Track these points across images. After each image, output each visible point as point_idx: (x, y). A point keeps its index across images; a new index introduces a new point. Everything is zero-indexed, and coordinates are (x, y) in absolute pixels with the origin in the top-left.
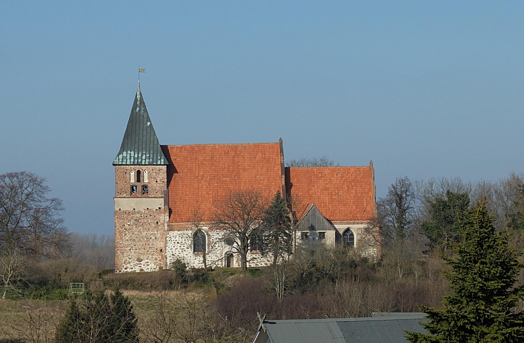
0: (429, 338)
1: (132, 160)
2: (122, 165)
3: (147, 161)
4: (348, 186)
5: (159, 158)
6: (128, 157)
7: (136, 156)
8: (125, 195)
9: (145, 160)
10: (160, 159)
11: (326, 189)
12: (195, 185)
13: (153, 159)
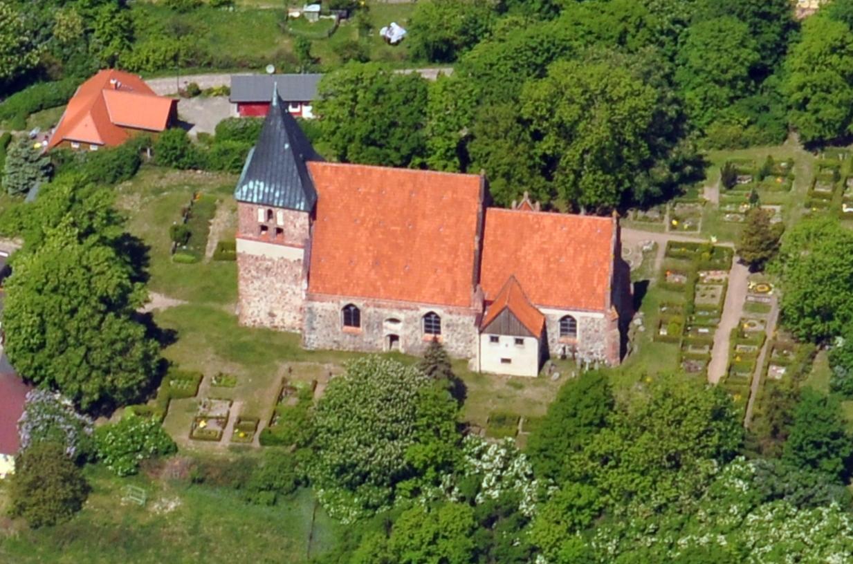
0: (800, 326)
1: (261, 197)
2: (245, 202)
3: (282, 201)
4: (575, 250)
5: (298, 199)
6: (256, 191)
7: (267, 190)
8: (251, 235)
9: (279, 198)
10: (300, 202)
11: (543, 251)
12: (351, 234)
13: (290, 199)
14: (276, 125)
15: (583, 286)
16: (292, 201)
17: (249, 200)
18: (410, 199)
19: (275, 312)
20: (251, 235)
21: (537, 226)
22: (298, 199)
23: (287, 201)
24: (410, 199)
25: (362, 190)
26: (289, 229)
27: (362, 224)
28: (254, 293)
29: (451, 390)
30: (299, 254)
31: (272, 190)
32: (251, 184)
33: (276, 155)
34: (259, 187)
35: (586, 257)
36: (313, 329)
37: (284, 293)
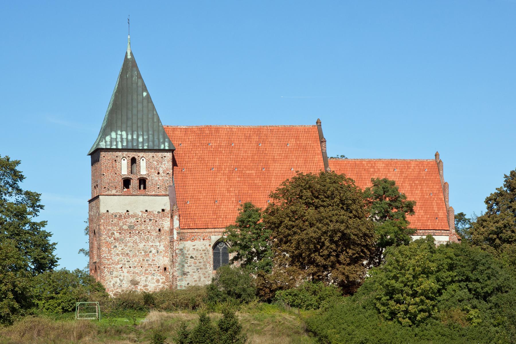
1: (125, 144)
5: (162, 140)
6: (119, 139)
7: (130, 137)
8: (114, 192)
9: (143, 143)
13: (153, 142)
14: (132, 76)
15: (426, 212)
16: (156, 142)
17: (114, 147)
18: (258, 148)
19: (138, 279)
20: (114, 192)
21: (372, 170)
22: (162, 140)
23: (151, 143)
24: (258, 148)
25: (213, 144)
26: (153, 179)
27: (218, 171)
28: (116, 259)
29: (342, 274)
30: (165, 203)
31: (135, 137)
32: (113, 135)
33: (135, 104)
34: (121, 135)
35: (422, 190)
36: (184, 274)
37: (147, 253)
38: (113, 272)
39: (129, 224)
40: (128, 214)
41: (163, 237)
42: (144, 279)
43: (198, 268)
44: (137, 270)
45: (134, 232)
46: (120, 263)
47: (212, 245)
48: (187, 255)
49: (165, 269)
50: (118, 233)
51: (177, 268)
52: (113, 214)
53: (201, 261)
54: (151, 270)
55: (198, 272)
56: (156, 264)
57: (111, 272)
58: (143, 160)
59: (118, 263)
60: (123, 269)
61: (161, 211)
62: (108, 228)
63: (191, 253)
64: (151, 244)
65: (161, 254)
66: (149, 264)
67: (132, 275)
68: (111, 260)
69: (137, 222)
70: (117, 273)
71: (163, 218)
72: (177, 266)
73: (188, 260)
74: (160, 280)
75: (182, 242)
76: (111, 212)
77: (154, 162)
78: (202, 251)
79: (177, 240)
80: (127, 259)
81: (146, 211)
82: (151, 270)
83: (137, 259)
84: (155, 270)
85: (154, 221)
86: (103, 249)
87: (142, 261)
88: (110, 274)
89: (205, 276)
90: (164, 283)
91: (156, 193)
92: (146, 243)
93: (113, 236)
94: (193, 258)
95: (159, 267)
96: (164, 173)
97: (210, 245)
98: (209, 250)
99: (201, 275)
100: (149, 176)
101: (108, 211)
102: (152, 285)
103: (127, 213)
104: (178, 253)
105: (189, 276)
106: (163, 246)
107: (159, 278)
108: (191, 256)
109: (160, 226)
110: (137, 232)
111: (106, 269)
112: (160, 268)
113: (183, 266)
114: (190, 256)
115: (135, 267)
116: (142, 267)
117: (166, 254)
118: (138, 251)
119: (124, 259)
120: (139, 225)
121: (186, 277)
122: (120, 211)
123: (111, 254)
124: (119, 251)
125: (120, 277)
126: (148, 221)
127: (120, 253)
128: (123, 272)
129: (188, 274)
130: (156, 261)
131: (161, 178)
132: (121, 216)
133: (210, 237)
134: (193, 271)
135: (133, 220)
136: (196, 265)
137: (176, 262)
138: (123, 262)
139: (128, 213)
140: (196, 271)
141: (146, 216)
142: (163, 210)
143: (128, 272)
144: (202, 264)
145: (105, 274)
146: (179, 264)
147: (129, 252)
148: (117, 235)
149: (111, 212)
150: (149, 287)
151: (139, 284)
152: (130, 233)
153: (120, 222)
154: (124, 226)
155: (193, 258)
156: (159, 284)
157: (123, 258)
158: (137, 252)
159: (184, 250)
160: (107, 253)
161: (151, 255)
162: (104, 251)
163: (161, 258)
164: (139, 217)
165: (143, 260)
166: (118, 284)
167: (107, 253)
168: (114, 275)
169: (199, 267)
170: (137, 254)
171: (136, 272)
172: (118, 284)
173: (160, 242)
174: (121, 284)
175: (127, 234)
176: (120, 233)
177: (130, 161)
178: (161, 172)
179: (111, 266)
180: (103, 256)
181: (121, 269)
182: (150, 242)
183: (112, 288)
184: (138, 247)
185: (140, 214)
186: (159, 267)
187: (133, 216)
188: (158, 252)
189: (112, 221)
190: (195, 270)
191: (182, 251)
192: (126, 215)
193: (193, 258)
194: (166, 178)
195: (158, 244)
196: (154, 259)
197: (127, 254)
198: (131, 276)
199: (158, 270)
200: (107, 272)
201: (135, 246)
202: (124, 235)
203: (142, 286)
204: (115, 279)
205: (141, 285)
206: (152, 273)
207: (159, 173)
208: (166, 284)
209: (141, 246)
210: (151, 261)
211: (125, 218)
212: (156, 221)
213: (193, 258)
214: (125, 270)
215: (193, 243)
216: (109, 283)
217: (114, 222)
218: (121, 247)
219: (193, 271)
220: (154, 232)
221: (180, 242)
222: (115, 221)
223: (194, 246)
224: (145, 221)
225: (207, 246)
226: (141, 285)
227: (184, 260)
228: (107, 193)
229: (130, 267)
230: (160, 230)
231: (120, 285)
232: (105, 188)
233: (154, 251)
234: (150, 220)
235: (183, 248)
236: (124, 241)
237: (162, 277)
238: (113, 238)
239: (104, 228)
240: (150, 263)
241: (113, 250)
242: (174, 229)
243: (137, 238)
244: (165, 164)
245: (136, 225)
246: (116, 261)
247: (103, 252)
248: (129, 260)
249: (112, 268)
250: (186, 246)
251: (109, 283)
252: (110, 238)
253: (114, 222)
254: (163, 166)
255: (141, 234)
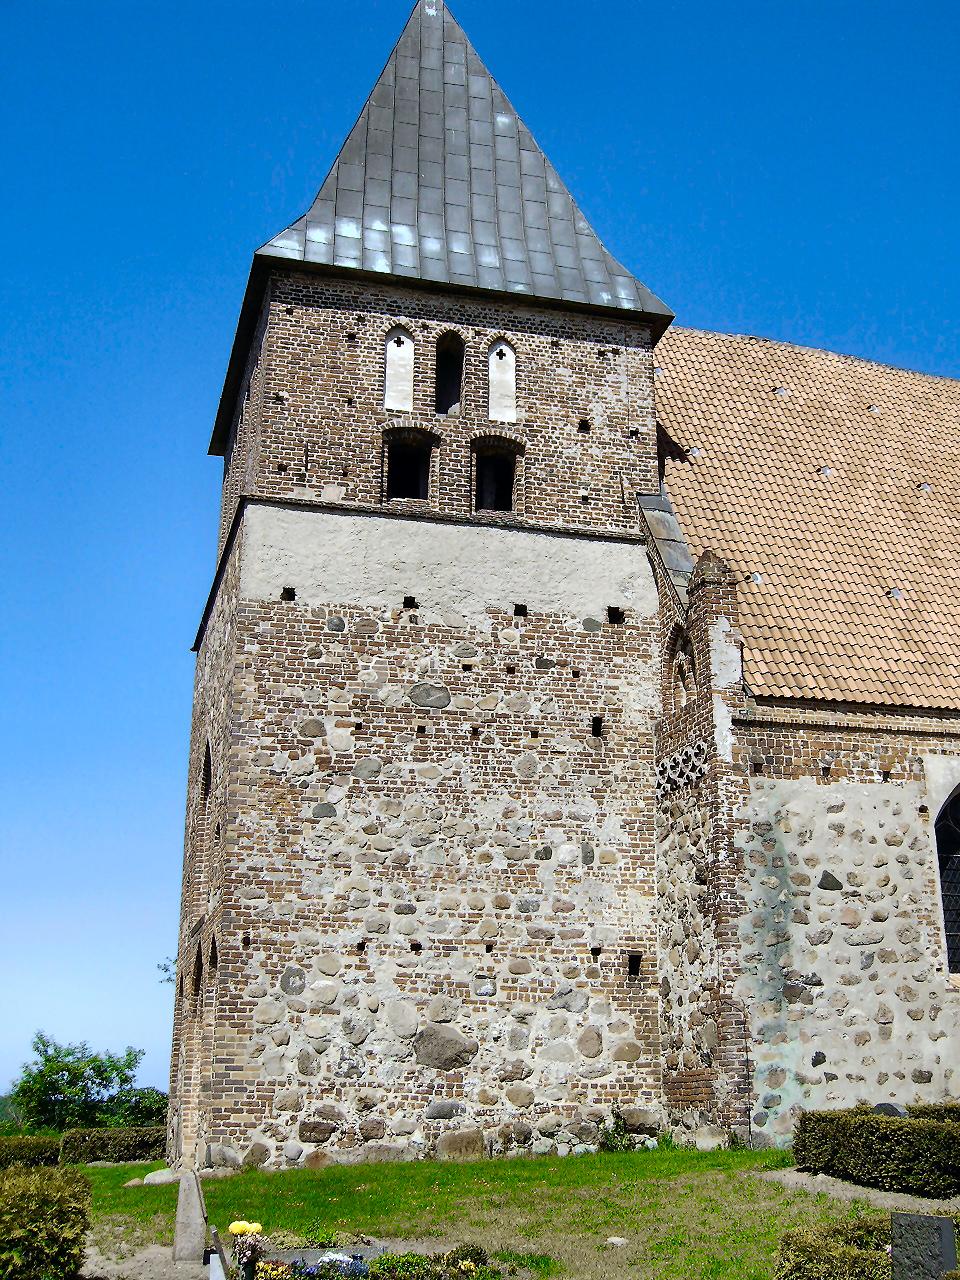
8: (333, 494)
19: (462, 1025)
28: (330, 890)
36: (792, 990)
38: (301, 976)
39: (416, 678)
40: (413, 619)
41: (617, 769)
42: (508, 1028)
43: (869, 949)
44: (459, 968)
45: (444, 725)
46: (350, 914)
47: (934, 813)
48: (803, 869)
49: (634, 963)
50: (349, 725)
51: (747, 949)
52: (318, 613)
53: (884, 905)
54: (546, 971)
55: (873, 977)
56: (581, 934)
57: (292, 972)
58: (501, 355)
59: (336, 920)
60: (372, 956)
61: (602, 617)
62: (288, 692)
63: (822, 857)
64: (550, 807)
65: (608, 870)
66: (535, 933)
67: (426, 996)
68: (292, 896)
69: (467, 668)
70: (328, 982)
71: (618, 660)
72: (747, 939)
73: (811, 901)
74: (606, 1033)
75: (759, 778)
76: (309, 599)
77: (559, 371)
78: (881, 841)
79: (736, 768)
80: (397, 894)
81: (521, 610)
82: (546, 971)
83: (464, 899)
84: (571, 973)
85: (567, 672)
86: (246, 819)
87: (490, 909)
88: (285, 987)
89: (912, 1006)
90: (627, 1054)
91: (572, 526)
92: (516, 796)
93: (318, 742)
94: (837, 886)
95: (596, 952)
96: (612, 428)
97: (923, 809)
98: (922, 838)
99: (891, 1000)
100: (533, 434)
101: (289, 594)
102: (555, 1066)
103: (405, 616)
104: (748, 847)
105: (820, 1006)
106: (618, 820)
107: (595, 1019)
108: (827, 876)
109: (600, 704)
110: (467, 726)
111: (262, 955)
112: (601, 957)
113: (783, 938)
114: (815, 874)
115: (449, 948)
116: (489, 949)
117: (640, 873)
118: (470, 847)
119: (378, 892)
120: (477, 691)
121: (802, 1015)
122: (368, 601)
123: (295, 855)
124: (351, 842)
125: (347, 1012)
126: (528, 666)
127: (353, 851)
128: (370, 980)
129: (816, 990)
130: (576, 912)
131: (595, 451)
132: (368, 625)
133: (920, 761)
134: (842, 969)
135: (438, 658)
136: (857, 935)
137: (738, 912)
138: (370, 913)
139: (411, 612)
140: (858, 972)
141: (517, 642)
142: (615, 615)
143: (400, 980)
144: (892, 925)
145: (252, 987)
146: (759, 924)
147: (413, 851)
148: (339, 738)
149: (309, 599)
150: (533, 1080)
151: (475, 1060)
152: (421, 729)
153: (360, 663)
154: (389, 687)
155: (838, 886)
156: (601, 1062)
157: (373, 884)
158: (460, 851)
159: (778, 832)
160: (271, 847)
161: (545, 871)
162: (249, 836)
163: (608, 891)
164: (479, 639)
165: (502, 905)
166: (333, 1055)
167: (271, 847)
168: (307, 998)
169: (874, 948)
170: (464, 861)
171: (456, 978)
172: (333, 1055)
173: (598, 795)
174: (356, 1060)
175: (403, 739)
176: (358, 726)
177: (431, 350)
178: (597, 422)
179: (292, 936)
180: (243, 868)
181: (355, 960)
182: (542, 795)
183: (295, 1087)
184: (469, 820)
185: (486, 625)
186: (596, 952)
187: (443, 635)
188: (588, 858)
189: (315, 654)
190: (855, 968)
191: (769, 835)
192: (401, 623)
193: (837, 886)
194: (625, 455)
195: (589, 807)
196: (565, 897)
197: (401, 864)
198: (421, 1004)
199: (592, 973)
200: (261, 973)
201: (451, 815)
202: (381, 741)
203: (490, 1075)
204: (317, 1024)
205: (485, 1069)
206: (556, 990)
207: (584, 426)
208: (642, 1059)
209: (488, 812)
210: (546, 909)
211: (392, 640)
212: (576, 674)
213: (838, 886)
214: (385, 968)
215: (832, 792)
216: (272, 1050)
217: (323, 660)
218: (367, 814)
219: (842, 969)
220: (567, 733)
221: (752, 781)
222: (334, 653)
223: (838, 808)
224: (511, 670)
225: (910, 814)
226: (485, 1069)
227: (782, 897)
228: (290, 495)
229: (416, 947)
230: (597, 727)
231: (345, 1067)
232: (282, 468)
233: (565, 851)
234: (543, 664)
235: (772, 821)
236: (381, 778)
237: (616, 1017)
238: (311, 758)
239: (264, 692)
240: (545, 925)
241: (312, 834)
242: (717, 699)
243: (465, 767)
244: (617, 384)
245: (455, 686)
246: (329, 899)
247: (244, 841)
248: (409, 899)
249: (298, 952)
250: (792, 806)
251: (272, 1050)
252: (294, 757)
253: (323, 660)
254: (607, 392)
255: (489, 740)
